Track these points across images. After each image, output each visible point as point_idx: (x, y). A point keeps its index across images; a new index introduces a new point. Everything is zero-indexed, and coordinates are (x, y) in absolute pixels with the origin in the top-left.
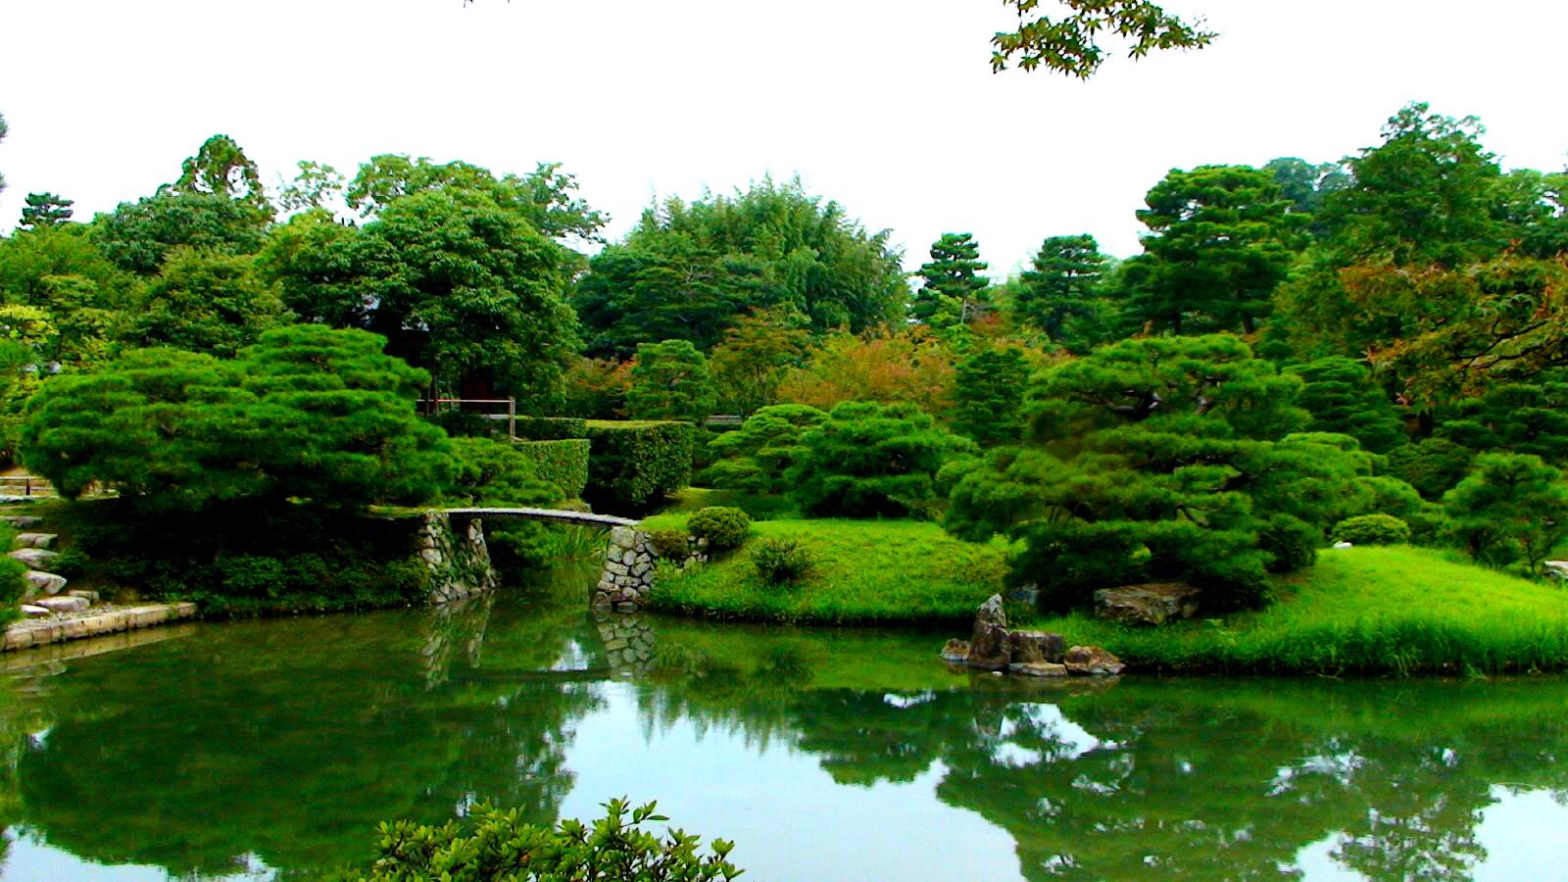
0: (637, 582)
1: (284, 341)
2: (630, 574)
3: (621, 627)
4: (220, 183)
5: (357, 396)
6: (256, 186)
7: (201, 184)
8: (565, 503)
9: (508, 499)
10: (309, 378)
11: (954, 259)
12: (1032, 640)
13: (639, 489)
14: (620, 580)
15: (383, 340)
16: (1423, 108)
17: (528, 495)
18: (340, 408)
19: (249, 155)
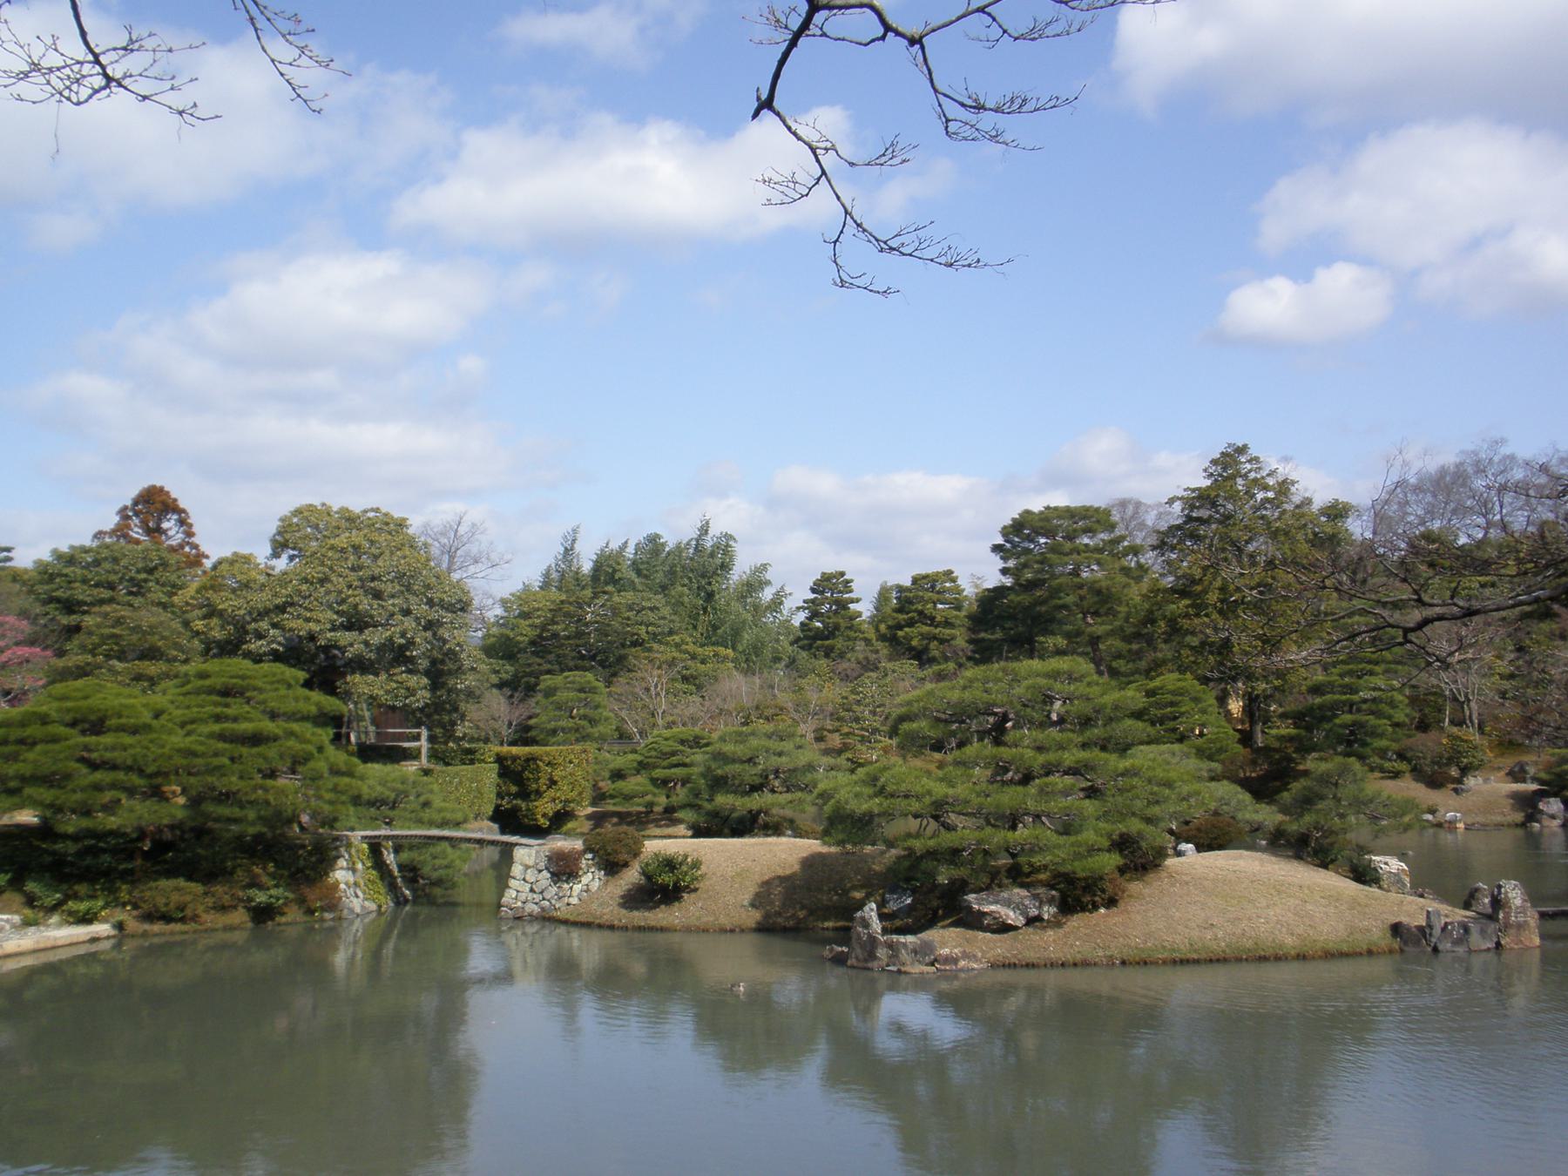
0: (538, 897)
1: (203, 675)
2: (532, 890)
3: (524, 934)
4: (155, 532)
5: (269, 726)
6: (190, 534)
7: (137, 533)
8: (476, 825)
9: (420, 822)
10: (229, 711)
11: (831, 587)
12: (904, 945)
13: (544, 807)
14: (523, 897)
15: (302, 675)
16: (1242, 450)
17: (437, 817)
18: (256, 739)
19: (182, 504)
